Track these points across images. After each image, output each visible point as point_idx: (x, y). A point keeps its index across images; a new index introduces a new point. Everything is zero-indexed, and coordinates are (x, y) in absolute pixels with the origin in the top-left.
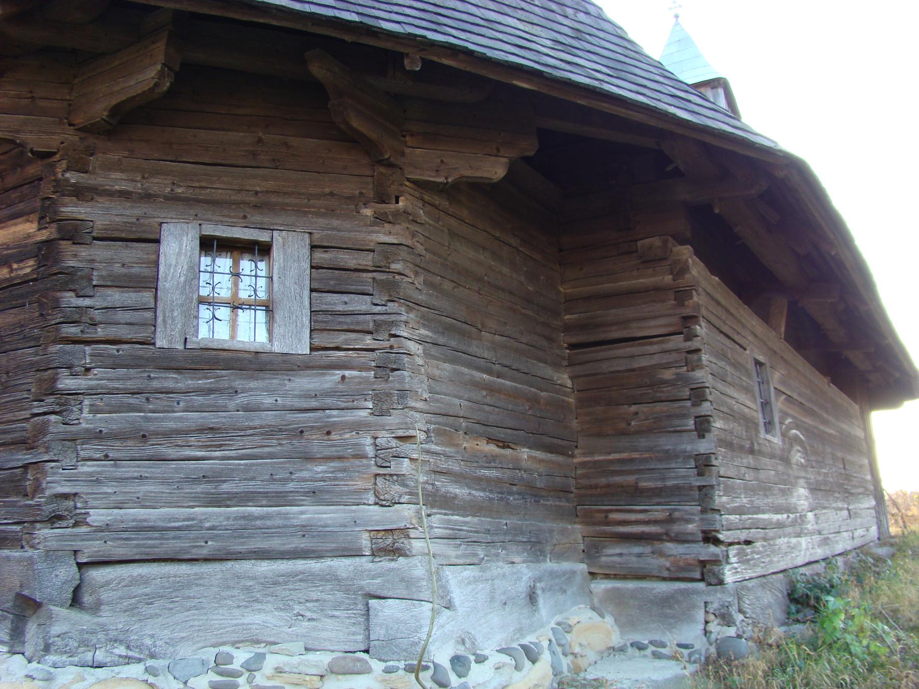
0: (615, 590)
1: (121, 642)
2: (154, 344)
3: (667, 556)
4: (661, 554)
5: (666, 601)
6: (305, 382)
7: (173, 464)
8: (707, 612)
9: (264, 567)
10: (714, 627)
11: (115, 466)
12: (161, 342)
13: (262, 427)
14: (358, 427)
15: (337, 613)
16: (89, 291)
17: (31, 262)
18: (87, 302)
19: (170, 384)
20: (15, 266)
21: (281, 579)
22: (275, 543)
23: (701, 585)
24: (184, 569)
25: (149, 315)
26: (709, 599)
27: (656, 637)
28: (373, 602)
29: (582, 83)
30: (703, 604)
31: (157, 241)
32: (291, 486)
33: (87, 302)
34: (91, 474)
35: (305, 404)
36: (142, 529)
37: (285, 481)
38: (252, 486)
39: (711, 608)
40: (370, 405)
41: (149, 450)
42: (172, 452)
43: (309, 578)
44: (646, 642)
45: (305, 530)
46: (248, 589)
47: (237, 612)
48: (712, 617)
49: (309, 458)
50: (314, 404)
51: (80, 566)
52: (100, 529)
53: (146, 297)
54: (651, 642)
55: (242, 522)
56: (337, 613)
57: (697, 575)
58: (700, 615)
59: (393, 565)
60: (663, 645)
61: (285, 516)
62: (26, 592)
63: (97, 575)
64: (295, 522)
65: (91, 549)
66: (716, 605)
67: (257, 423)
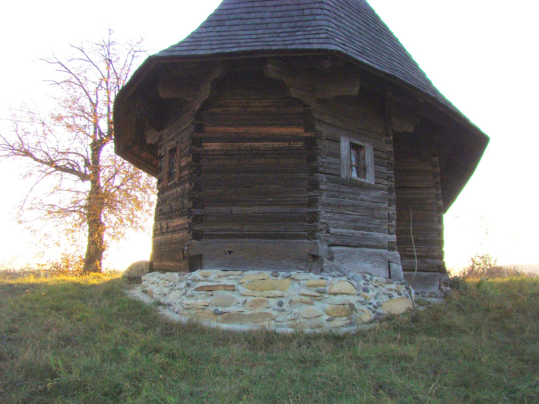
0: (407, 274)
1: (338, 270)
2: (340, 176)
3: (427, 263)
4: (424, 263)
5: (426, 278)
6: (373, 194)
7: (347, 216)
8: (440, 282)
9: (368, 250)
10: (443, 287)
11: (334, 215)
12: (342, 176)
13: (365, 206)
14: (385, 209)
15: (383, 266)
16: (324, 157)
17: (301, 143)
18: (324, 160)
19: (344, 190)
20: (292, 143)
21: (371, 254)
22: (370, 243)
23: (439, 274)
24: (349, 249)
25: (338, 166)
26: (441, 277)
27: (422, 290)
28: (390, 263)
29: (461, 113)
30: (439, 280)
31: (339, 142)
32: (371, 226)
33: (324, 160)
34: (329, 217)
35: (373, 200)
36: (342, 235)
37: (371, 224)
38: (363, 225)
39: (442, 281)
40: (387, 202)
41: (341, 211)
42: (346, 212)
43: (377, 254)
44: (419, 292)
45: (376, 239)
46: (364, 256)
47: (362, 263)
48: (442, 284)
49: (375, 217)
50: (376, 201)
51: (329, 245)
52: (333, 234)
53: (338, 160)
54: (421, 292)
55: (362, 236)
56: (383, 266)
57: (437, 270)
58: (438, 283)
59: (393, 253)
60: (425, 293)
61: (371, 235)
62: (313, 253)
63: (334, 248)
64: (373, 237)
65: (332, 240)
66: (444, 280)
67: (364, 205)
